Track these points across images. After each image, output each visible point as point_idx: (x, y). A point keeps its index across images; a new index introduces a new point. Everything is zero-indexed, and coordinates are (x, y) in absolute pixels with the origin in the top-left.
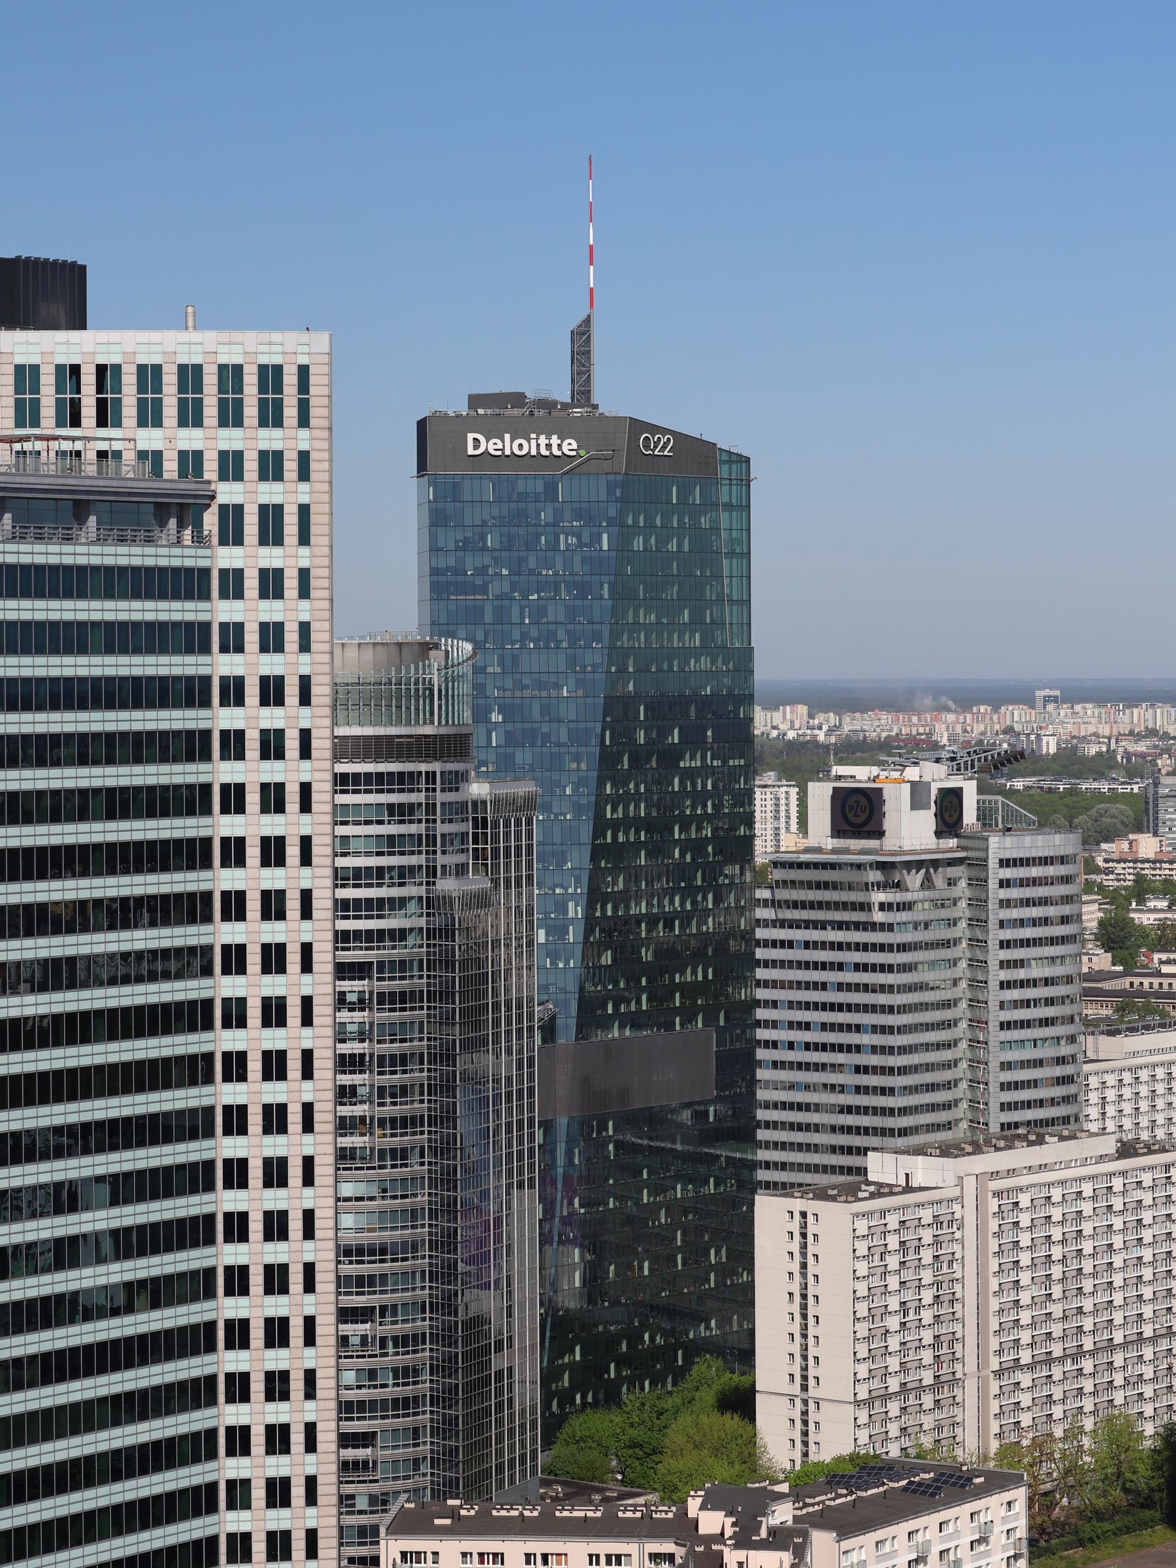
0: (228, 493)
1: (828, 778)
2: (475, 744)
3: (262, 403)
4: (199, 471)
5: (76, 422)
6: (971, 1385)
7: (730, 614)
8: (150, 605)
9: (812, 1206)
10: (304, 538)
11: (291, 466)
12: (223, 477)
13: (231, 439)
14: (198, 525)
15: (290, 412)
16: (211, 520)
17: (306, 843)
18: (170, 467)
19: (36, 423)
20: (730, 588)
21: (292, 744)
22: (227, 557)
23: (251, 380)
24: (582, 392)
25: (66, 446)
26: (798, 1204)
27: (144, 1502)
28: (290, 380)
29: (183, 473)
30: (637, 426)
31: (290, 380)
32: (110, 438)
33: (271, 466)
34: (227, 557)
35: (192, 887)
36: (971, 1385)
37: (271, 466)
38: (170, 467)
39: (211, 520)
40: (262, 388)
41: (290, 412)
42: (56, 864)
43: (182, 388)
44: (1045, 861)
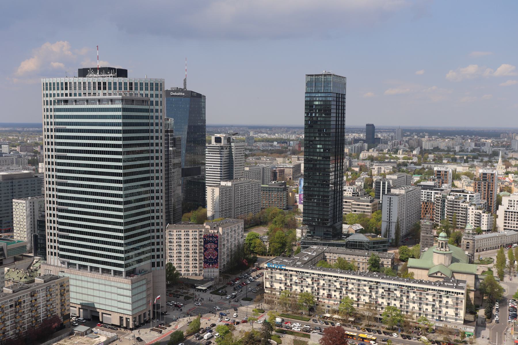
0: (152, 99)
1: (214, 135)
2: (299, 156)
3: (156, 88)
4: (148, 96)
5: (132, 90)
6: (233, 209)
7: (203, 115)
8: (142, 113)
9: (214, 188)
10: (161, 105)
11: (159, 96)
12: (151, 97)
13: (152, 92)
14: (148, 103)
15: (159, 89)
16: (149, 103)
17: (161, 143)
18: (144, 95)
19: (127, 90)
20: (203, 112)
21: (159, 131)
22: (151, 107)
23: (154, 85)
24: (185, 88)
25: (130, 93)
26: (212, 188)
27: (128, 211)
28: (159, 85)
29: (146, 97)
30: (192, 92)
31: (159, 85)
32: (137, 92)
33: (157, 96)
34: (151, 107)
35: (125, 141)
36: (233, 209)
37: (157, 96)
38: (144, 95)
39: (149, 103)
40: (140, 85)
41: (159, 89)
42: (108, 138)
43: (116, 87)
44: (241, 146)
